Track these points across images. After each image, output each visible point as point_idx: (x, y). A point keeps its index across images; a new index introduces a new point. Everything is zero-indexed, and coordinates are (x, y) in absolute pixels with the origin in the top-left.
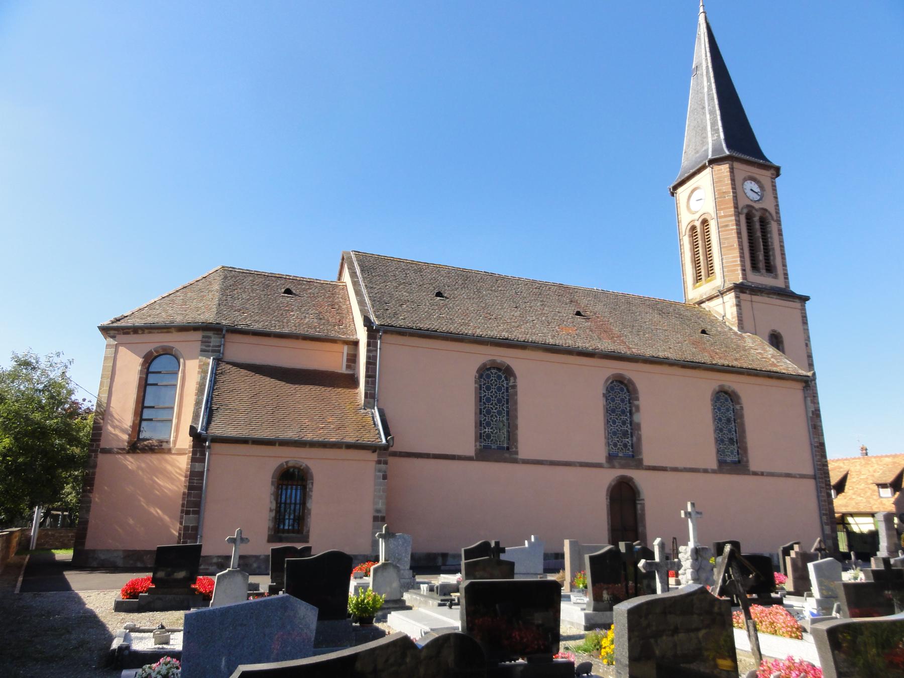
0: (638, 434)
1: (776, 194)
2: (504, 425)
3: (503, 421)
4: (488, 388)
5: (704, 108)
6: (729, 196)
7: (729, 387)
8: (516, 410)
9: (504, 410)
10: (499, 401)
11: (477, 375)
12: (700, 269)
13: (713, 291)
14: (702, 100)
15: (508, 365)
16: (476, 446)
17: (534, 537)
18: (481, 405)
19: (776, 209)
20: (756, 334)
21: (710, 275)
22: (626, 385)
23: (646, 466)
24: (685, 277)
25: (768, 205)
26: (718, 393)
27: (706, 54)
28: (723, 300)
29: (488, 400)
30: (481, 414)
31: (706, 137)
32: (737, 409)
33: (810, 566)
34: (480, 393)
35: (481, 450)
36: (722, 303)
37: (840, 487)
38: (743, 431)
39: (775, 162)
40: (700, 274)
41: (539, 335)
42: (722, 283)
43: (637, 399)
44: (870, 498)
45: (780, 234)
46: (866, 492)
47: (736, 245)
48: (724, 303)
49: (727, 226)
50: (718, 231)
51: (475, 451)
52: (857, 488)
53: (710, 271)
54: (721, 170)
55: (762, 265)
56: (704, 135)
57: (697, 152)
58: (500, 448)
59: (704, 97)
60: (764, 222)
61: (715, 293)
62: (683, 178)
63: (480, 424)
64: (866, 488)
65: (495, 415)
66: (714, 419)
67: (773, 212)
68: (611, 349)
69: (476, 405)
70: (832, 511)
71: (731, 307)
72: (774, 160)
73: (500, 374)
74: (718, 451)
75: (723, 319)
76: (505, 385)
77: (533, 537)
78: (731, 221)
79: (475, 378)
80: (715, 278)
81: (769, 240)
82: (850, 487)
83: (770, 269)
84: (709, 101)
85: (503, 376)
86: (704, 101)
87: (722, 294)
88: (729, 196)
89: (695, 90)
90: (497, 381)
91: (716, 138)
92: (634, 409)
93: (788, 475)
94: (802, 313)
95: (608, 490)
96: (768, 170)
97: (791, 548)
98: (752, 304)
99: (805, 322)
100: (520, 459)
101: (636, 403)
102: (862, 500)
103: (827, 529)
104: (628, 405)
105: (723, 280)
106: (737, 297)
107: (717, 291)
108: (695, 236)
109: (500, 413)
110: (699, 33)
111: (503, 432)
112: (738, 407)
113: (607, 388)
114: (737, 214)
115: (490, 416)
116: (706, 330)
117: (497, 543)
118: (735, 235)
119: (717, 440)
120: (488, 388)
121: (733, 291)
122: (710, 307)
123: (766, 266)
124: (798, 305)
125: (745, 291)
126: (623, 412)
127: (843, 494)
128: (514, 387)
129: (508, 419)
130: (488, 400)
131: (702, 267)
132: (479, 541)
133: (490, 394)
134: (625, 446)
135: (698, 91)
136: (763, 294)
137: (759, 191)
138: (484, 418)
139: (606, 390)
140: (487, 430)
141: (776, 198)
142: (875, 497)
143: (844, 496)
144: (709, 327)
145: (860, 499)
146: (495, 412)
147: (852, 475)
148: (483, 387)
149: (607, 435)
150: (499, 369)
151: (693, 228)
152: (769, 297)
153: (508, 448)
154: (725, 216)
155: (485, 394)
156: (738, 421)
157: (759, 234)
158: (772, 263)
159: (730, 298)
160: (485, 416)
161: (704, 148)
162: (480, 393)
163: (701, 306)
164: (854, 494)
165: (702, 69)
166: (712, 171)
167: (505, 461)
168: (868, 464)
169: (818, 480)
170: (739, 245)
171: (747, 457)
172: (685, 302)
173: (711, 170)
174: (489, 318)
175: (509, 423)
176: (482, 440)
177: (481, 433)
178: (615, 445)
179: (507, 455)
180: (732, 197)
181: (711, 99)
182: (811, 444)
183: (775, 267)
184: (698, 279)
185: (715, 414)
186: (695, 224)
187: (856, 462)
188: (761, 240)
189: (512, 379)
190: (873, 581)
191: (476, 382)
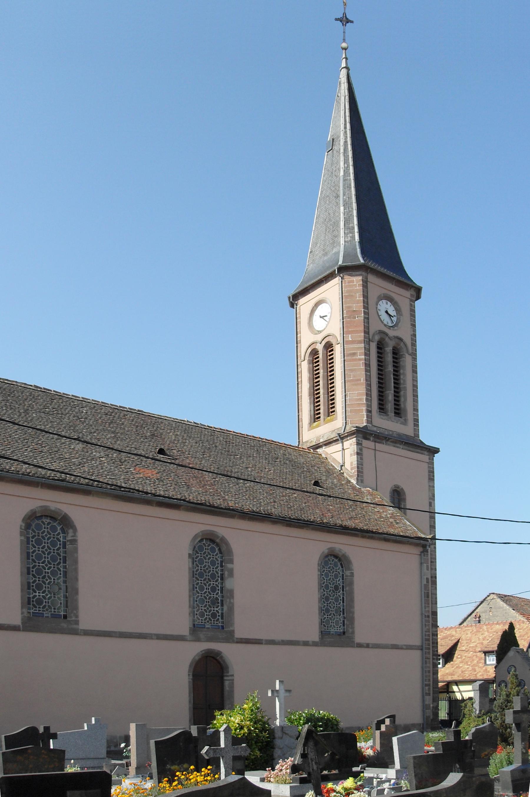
0: (230, 602)
1: (414, 321)
2: (60, 589)
3: (58, 584)
4: (38, 542)
5: (337, 196)
6: (360, 316)
7: (340, 550)
8: (76, 570)
9: (60, 571)
10: (54, 559)
11: (24, 525)
12: (319, 405)
13: (332, 433)
14: (337, 185)
15: (65, 513)
16: (22, 613)
17: (95, 720)
18: (28, 563)
19: (412, 340)
20: (377, 490)
21: (330, 414)
22: (218, 545)
23: (237, 638)
24: (300, 413)
25: (404, 333)
26: (327, 556)
27: (345, 124)
28: (343, 446)
29: (39, 557)
30: (28, 573)
31: (337, 236)
32: (347, 576)
33: (395, 740)
34: (28, 548)
35: (29, 619)
36: (341, 449)
37: (449, 656)
38: (352, 600)
39: (417, 281)
40: (318, 412)
41: (108, 477)
42: (343, 426)
43: (231, 562)
44: (476, 666)
45: (415, 371)
46: (473, 660)
47: (363, 380)
48: (343, 449)
49: (354, 354)
50: (343, 359)
51: (22, 619)
52: (465, 656)
53: (331, 410)
54: (353, 281)
55: (390, 406)
56: (336, 233)
57: (326, 254)
58: (55, 616)
59: (339, 181)
60: (396, 353)
61: (334, 435)
62: (306, 286)
63: (27, 587)
64: (474, 656)
65: (48, 576)
66: (320, 586)
67: (408, 342)
68: (201, 500)
69: (22, 562)
70: (436, 681)
71: (351, 455)
72: (417, 279)
73: (55, 524)
74: (322, 622)
75: (342, 469)
76: (61, 539)
77: (93, 719)
78: (358, 348)
79: (21, 528)
80: (336, 419)
81: (402, 377)
82: (459, 655)
83: (398, 412)
84: (344, 188)
85: (59, 528)
86: (339, 187)
87: (342, 439)
88: (360, 316)
89: (328, 170)
90: (50, 534)
91: (349, 239)
92: (226, 573)
93: (395, 647)
94: (429, 467)
95: (190, 666)
96: (407, 290)
97: (383, 722)
98: (375, 452)
99: (431, 478)
100: (81, 630)
101: (229, 566)
102: (468, 668)
103: (429, 700)
104: (219, 568)
105: (345, 421)
106: (358, 444)
107: (337, 435)
108: (316, 362)
109: (54, 573)
110: (339, 95)
111: (58, 598)
112: (348, 573)
113: (195, 547)
114: (368, 341)
115: (41, 577)
116: (319, 481)
117: (47, 729)
118: (363, 367)
119: (321, 610)
120: (38, 542)
121: (355, 436)
122: (327, 453)
123: (395, 408)
124: (425, 457)
125: (368, 437)
126: (213, 576)
127: (452, 663)
128: (74, 541)
129: (65, 582)
130: (39, 557)
131: (321, 403)
132: (24, 727)
133: (41, 550)
134: (214, 615)
135: (332, 173)
136: (389, 443)
137: (395, 315)
138: (34, 579)
139: (193, 550)
140: (37, 594)
141: (414, 326)
142: (481, 665)
143: (452, 665)
144: (324, 478)
145: (466, 667)
146: (48, 573)
147: (463, 643)
148: (32, 541)
149: (192, 603)
150: (53, 518)
151: (314, 353)
152: (394, 446)
153: (65, 617)
154: (353, 342)
155: (34, 549)
156: (347, 588)
157: (390, 368)
158: (402, 406)
159: (351, 444)
160: (35, 577)
161: (335, 250)
162: (28, 548)
163: (317, 452)
164: (462, 662)
165: (339, 144)
166: (342, 281)
167: (63, 631)
168: (479, 632)
169: (424, 651)
170: (366, 380)
171: (353, 628)
172: (299, 445)
173: (340, 280)
174: (40, 450)
175: (66, 586)
176: (31, 606)
177: (29, 598)
178: (202, 615)
179: (64, 625)
180: (363, 319)
181: (347, 187)
182: (422, 614)
183: (405, 410)
184: (315, 417)
185: (321, 581)
186: (317, 347)
187: (468, 630)
188: (392, 376)
189: (71, 531)
190: (442, 752)
191: (21, 534)
